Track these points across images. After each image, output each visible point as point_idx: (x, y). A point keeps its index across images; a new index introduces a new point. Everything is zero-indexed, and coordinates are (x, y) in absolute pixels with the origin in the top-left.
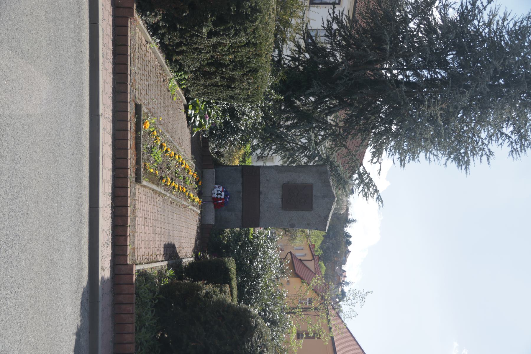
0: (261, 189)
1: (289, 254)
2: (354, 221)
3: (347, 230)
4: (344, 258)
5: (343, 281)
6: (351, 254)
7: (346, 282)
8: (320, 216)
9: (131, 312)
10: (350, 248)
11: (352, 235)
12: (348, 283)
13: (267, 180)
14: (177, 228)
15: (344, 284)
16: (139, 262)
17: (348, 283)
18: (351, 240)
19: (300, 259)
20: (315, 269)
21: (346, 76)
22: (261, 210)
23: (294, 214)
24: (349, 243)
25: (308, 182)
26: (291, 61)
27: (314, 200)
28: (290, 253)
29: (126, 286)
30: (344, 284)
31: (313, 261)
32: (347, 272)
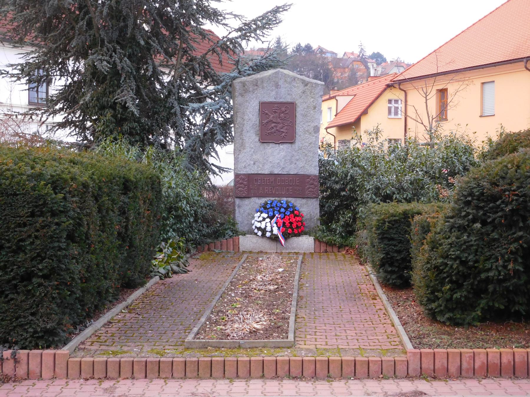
0: (267, 172)
1: (329, 130)
2: (278, 42)
3: (289, 51)
4: (329, 55)
5: (359, 56)
6: (322, 46)
7: (360, 52)
8: (304, 92)
9: (472, 354)
10: (315, 47)
11: (297, 43)
12: (362, 49)
13: (254, 164)
14: (333, 289)
15: (363, 55)
16: (296, 335)
17: (362, 49)
18: (303, 45)
19: (336, 116)
20: (348, 95)
21: (111, 56)
22: (295, 173)
23: (301, 127)
24: (308, 48)
25: (258, 107)
26: (75, 129)
27: (281, 100)
28: (326, 129)
29: (436, 361)
30: (363, 55)
31: (337, 98)
32: (347, 51)
